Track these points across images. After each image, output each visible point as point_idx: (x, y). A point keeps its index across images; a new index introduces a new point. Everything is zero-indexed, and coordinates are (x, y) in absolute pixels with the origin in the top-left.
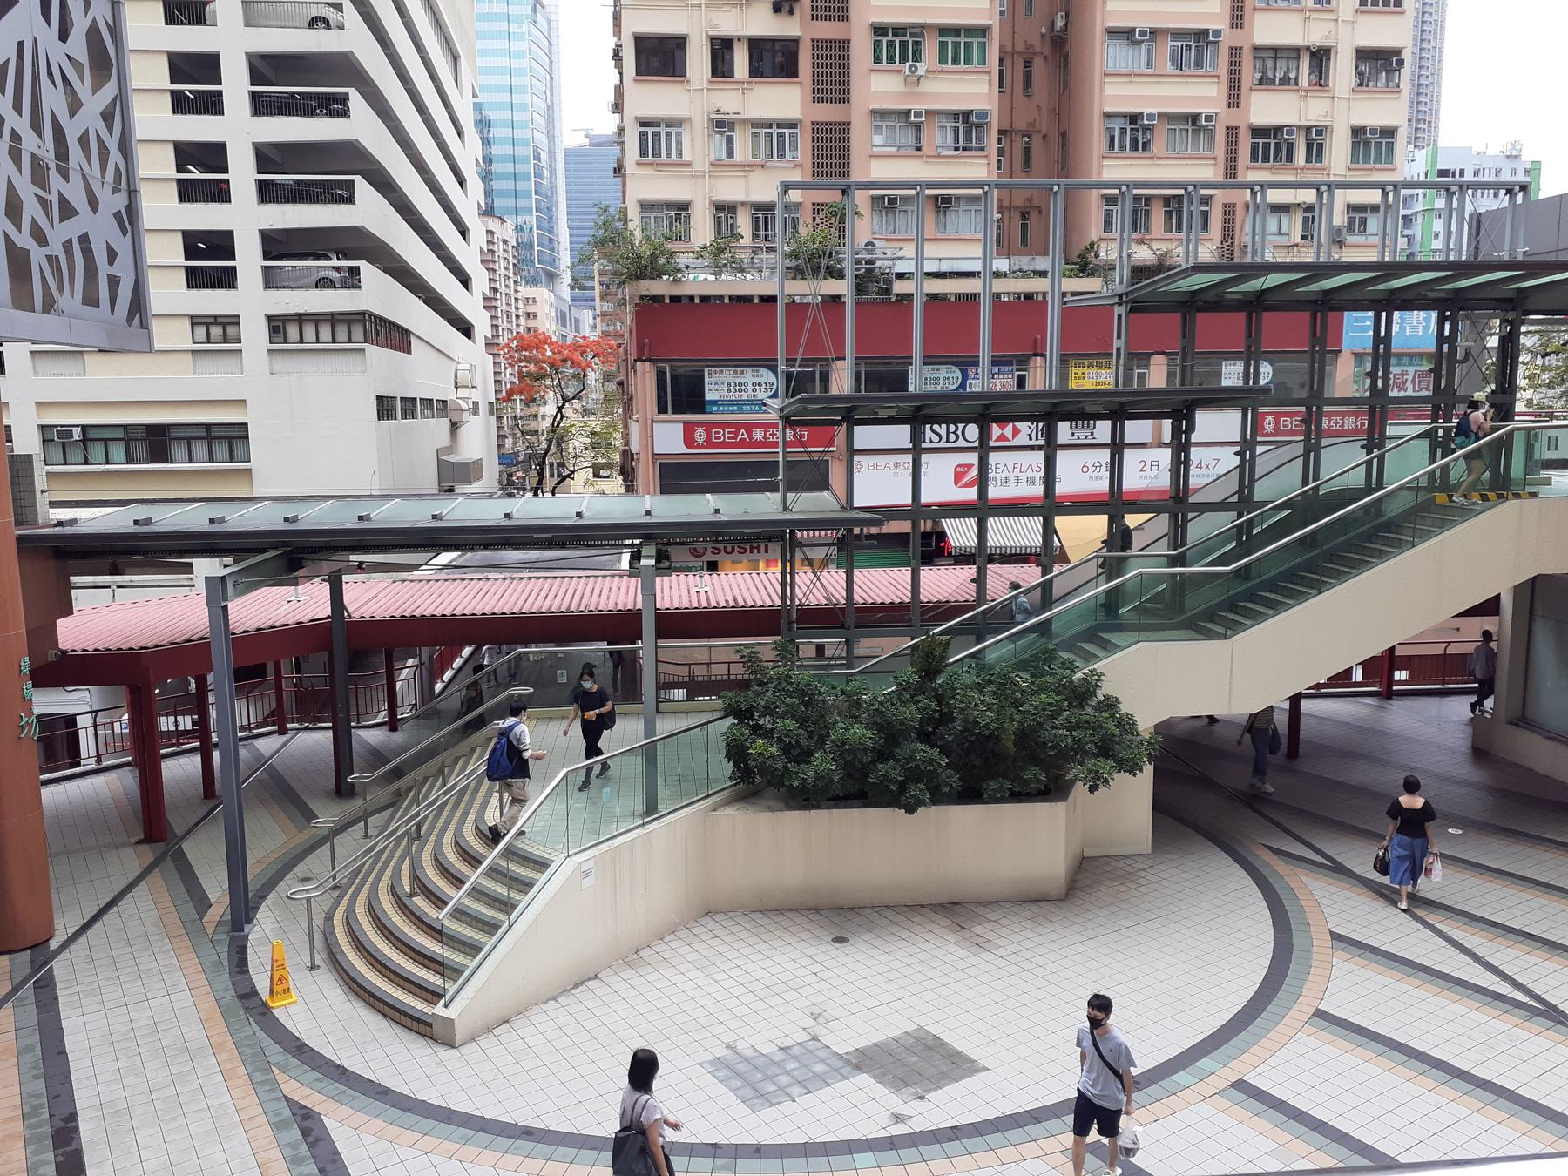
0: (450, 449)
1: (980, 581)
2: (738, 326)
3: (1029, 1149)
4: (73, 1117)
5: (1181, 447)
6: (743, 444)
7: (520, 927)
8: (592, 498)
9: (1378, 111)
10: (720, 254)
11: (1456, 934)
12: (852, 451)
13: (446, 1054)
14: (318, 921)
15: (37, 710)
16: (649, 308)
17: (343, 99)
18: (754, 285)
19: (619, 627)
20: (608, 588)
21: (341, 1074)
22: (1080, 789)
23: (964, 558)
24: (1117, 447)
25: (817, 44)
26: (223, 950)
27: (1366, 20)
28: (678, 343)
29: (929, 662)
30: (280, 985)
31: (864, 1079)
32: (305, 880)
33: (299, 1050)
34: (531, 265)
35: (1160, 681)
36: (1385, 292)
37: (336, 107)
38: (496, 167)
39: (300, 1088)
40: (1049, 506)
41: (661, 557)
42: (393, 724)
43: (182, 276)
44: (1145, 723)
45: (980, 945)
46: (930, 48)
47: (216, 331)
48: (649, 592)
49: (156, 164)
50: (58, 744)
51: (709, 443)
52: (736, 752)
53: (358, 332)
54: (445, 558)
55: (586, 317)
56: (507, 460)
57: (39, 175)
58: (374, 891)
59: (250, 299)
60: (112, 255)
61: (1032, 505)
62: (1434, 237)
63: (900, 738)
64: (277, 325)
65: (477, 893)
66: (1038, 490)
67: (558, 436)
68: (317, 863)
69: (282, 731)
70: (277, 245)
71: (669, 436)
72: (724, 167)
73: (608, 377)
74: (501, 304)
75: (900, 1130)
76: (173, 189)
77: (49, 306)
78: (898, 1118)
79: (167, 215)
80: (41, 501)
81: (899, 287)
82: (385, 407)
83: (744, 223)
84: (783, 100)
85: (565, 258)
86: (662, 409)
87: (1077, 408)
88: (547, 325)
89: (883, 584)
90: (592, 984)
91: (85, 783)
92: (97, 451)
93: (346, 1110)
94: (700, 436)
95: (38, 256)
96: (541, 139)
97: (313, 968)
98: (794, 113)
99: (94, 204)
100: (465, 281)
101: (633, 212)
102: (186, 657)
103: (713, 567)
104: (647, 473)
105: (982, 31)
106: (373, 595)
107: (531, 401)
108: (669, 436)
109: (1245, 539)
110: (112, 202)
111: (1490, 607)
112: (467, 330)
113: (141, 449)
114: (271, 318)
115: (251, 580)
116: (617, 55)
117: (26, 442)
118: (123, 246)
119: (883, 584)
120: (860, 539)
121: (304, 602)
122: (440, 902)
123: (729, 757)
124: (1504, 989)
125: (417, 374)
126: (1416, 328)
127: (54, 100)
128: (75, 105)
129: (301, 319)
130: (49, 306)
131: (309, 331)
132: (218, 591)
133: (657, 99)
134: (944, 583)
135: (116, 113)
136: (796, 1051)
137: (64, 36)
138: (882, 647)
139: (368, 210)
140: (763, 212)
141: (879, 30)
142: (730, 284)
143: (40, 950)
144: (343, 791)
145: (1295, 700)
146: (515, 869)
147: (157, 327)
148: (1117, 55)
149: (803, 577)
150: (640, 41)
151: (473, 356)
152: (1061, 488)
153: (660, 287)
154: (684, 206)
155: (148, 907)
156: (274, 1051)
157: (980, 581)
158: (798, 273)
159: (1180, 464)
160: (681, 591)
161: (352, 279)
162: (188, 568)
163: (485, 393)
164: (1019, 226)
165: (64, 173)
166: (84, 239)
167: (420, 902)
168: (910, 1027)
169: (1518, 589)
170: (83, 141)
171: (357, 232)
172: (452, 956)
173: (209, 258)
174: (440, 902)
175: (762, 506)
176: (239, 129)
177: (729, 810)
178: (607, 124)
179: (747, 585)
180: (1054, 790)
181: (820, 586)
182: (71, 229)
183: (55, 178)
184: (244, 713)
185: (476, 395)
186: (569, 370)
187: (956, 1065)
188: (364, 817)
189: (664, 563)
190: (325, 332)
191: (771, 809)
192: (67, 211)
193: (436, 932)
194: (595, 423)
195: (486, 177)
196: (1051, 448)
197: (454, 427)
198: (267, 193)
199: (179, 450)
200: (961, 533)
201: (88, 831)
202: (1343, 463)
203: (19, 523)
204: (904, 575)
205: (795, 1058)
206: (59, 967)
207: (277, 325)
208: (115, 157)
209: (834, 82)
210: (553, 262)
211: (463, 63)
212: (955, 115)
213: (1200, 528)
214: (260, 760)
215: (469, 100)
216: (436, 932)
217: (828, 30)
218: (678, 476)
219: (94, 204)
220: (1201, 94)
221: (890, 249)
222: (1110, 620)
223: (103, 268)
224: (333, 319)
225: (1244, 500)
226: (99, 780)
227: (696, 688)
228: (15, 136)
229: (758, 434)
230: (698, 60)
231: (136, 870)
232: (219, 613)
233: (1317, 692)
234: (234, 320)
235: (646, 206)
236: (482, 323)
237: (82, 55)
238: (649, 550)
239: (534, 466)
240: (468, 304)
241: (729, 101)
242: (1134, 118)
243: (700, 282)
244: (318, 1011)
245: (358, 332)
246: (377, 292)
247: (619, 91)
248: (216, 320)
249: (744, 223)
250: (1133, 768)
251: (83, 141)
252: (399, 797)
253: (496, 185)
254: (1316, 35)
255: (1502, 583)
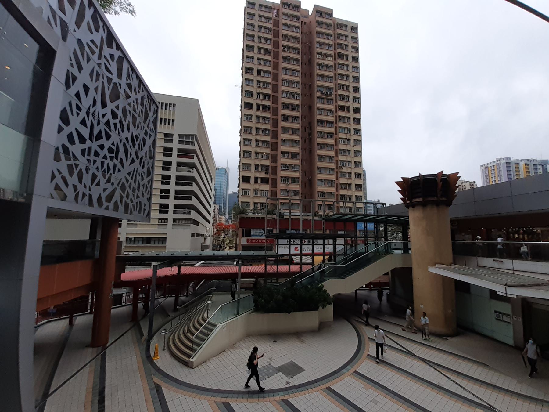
0: (204, 243)
1: (301, 268)
2: (258, 223)
3: (315, 389)
4: (104, 388)
5: (334, 245)
6: (257, 242)
7: (209, 340)
8: (229, 251)
9: (359, 194)
10: (255, 210)
11: (390, 337)
12: (278, 245)
13: (191, 370)
14: (166, 339)
15: (114, 293)
16: (242, 219)
17: (192, 183)
18: (260, 215)
19: (234, 276)
20: (232, 268)
21: (167, 376)
22: (321, 308)
23: (297, 264)
24: (324, 245)
25: (272, 179)
26: (145, 346)
27: (356, 180)
28: (246, 224)
29: (293, 282)
30: (156, 355)
31: (280, 373)
32: (165, 330)
33: (158, 370)
34: (221, 212)
35: (334, 287)
36: (366, 219)
37: (191, 185)
38: (217, 196)
39: (157, 380)
40: (313, 255)
41: (242, 262)
42: (187, 296)
43: (158, 211)
44: (331, 295)
45: (303, 342)
46: (290, 181)
47: (163, 221)
48: (240, 269)
49: (156, 192)
50: (118, 300)
51: (251, 242)
52: (255, 301)
53: (189, 222)
54: (202, 262)
55: (230, 221)
56: (214, 245)
57: (134, 190)
58: (179, 332)
59: (170, 216)
60: (145, 205)
61: (309, 255)
62: (371, 211)
63: (284, 300)
64: (175, 220)
65: (201, 332)
66: (311, 252)
67: (223, 241)
68: (168, 326)
69: (164, 297)
70: (179, 164)
71: (244, 241)
72: (257, 197)
73: (233, 231)
74: (215, 218)
75: (288, 386)
76: (159, 196)
77: (131, 213)
78: (288, 383)
79: (156, 200)
80: (123, 250)
81: (285, 217)
82: (193, 235)
83: (259, 206)
84: (266, 187)
85: (227, 210)
86: (243, 236)
87: (318, 237)
88: (223, 222)
89: (283, 268)
90: (224, 353)
91: (121, 308)
92: (136, 242)
93: (167, 385)
94: (250, 241)
95: (131, 204)
96: (225, 192)
97: (164, 350)
98: (268, 189)
99: (143, 196)
100: (210, 214)
101: (240, 203)
102: (146, 282)
103: (251, 265)
104: (239, 247)
105: (298, 178)
106: (186, 270)
107: (219, 235)
108: (244, 241)
109: (346, 261)
110: (147, 196)
111: (387, 274)
112: (209, 222)
113: (145, 242)
114: (174, 219)
115: (161, 266)
116: (239, 179)
117: (123, 239)
118: (148, 204)
119: (283, 268)
120: (279, 260)
121: (172, 271)
122: (193, 334)
123: (254, 302)
124: (401, 348)
125: (200, 230)
126: (371, 226)
127: (139, 178)
128: (143, 179)
129: (179, 219)
130: (131, 213)
131: (181, 222)
132: (155, 268)
133: (246, 186)
134: (294, 268)
135: (151, 182)
136: (266, 367)
137: (143, 168)
138: (282, 280)
139: (194, 201)
140: (262, 204)
141: (282, 177)
142: (256, 215)
143: (104, 348)
144: (175, 310)
145: (356, 291)
146: (210, 327)
147: (151, 220)
148: (319, 183)
149: (269, 267)
150: (243, 177)
151: (210, 227)
152: (300, 257)
153: (244, 215)
154: (249, 203)
155: (129, 337)
156: (153, 370)
157: (301, 268)
158: (268, 214)
159: (334, 248)
160: (246, 269)
161: (190, 213)
162: (151, 264)
163: (211, 233)
164: (306, 208)
165: (139, 191)
166: (140, 202)
167: (189, 334)
168: (289, 361)
169: (391, 271)
170: (143, 185)
171: (192, 205)
172: (195, 347)
173: (164, 208)
174: (193, 334)
175: (262, 253)
176: (175, 146)
177: (253, 314)
178: (236, 190)
179: (258, 268)
180: (316, 309)
181: (272, 269)
182: (138, 200)
183: (137, 191)
184: (157, 294)
185: (209, 234)
186: (227, 229)
187: (299, 370)
188: (179, 316)
189: (243, 264)
190: (184, 222)
191: (262, 313)
192: (138, 197)
193: (191, 341)
194: (230, 239)
195: (215, 198)
196: (313, 245)
197: (205, 239)
198: (177, 184)
199: (152, 242)
200: (297, 259)
201: (121, 319)
202: (361, 248)
203: (117, 254)
204: (287, 267)
205: (266, 369)
206: (107, 350)
207: (175, 220)
208: (149, 188)
209: (274, 184)
210: (225, 212)
211: (213, 180)
212: (294, 190)
213: (339, 259)
214: (159, 303)
215: (213, 185)
216: (191, 341)
217: (274, 177)
218: (244, 248)
219: (143, 196)
220: (333, 190)
221: (283, 211)
222: (323, 275)
223: (143, 207)
224: (185, 219)
225: (345, 254)
226: (125, 308)
227: (246, 289)
228: (130, 183)
229: (260, 241)
230: (252, 180)
231: (129, 327)
232: (155, 272)
233: (359, 290)
234: (167, 219)
235: (242, 202)
236: (212, 221)
237: (146, 172)
238: (240, 261)
239: (219, 246)
240: (210, 218)
241: (257, 187)
242: (322, 192)
243: (251, 215)
244: (164, 361)
245: (189, 222)
246: (194, 215)
247: (239, 184)
248: (163, 219)
249: (259, 206)
250: (330, 304)
251: (143, 185)
252: (186, 311)
253: (217, 199)
254: (349, 182)
255: (389, 270)
